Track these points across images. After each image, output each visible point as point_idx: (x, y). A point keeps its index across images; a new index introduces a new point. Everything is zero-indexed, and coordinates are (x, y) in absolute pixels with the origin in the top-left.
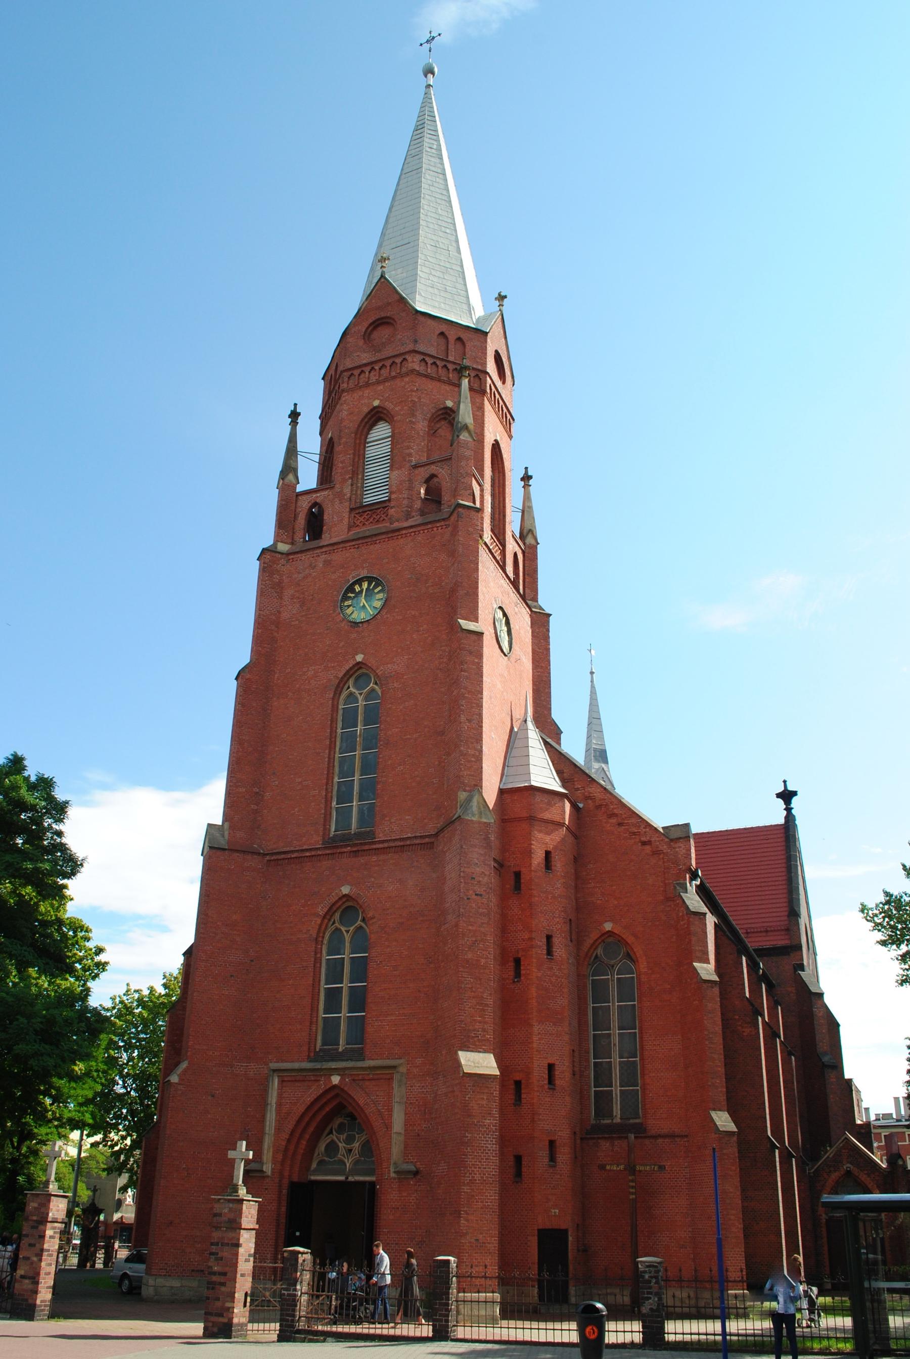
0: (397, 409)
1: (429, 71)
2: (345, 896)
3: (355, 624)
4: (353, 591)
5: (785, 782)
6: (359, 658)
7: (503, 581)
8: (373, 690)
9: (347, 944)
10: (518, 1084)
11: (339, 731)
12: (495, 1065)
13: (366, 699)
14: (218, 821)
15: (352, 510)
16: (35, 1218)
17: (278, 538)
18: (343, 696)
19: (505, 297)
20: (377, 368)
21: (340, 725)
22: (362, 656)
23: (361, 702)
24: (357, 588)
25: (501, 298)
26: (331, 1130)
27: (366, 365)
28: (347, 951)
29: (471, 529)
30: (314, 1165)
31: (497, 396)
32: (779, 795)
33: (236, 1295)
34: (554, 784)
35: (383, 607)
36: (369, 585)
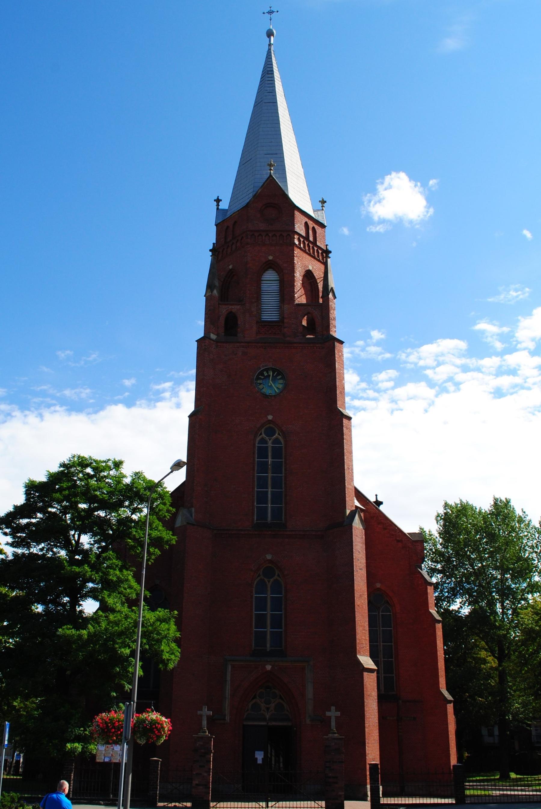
0: (285, 265)
1: (270, 34)
2: (268, 560)
3: (266, 396)
4: (263, 375)
5: (376, 495)
8: (277, 439)
9: (269, 589)
12: (373, 663)
16: (202, 751)
18: (258, 439)
19: (325, 202)
22: (272, 417)
23: (270, 444)
25: (323, 202)
28: (269, 593)
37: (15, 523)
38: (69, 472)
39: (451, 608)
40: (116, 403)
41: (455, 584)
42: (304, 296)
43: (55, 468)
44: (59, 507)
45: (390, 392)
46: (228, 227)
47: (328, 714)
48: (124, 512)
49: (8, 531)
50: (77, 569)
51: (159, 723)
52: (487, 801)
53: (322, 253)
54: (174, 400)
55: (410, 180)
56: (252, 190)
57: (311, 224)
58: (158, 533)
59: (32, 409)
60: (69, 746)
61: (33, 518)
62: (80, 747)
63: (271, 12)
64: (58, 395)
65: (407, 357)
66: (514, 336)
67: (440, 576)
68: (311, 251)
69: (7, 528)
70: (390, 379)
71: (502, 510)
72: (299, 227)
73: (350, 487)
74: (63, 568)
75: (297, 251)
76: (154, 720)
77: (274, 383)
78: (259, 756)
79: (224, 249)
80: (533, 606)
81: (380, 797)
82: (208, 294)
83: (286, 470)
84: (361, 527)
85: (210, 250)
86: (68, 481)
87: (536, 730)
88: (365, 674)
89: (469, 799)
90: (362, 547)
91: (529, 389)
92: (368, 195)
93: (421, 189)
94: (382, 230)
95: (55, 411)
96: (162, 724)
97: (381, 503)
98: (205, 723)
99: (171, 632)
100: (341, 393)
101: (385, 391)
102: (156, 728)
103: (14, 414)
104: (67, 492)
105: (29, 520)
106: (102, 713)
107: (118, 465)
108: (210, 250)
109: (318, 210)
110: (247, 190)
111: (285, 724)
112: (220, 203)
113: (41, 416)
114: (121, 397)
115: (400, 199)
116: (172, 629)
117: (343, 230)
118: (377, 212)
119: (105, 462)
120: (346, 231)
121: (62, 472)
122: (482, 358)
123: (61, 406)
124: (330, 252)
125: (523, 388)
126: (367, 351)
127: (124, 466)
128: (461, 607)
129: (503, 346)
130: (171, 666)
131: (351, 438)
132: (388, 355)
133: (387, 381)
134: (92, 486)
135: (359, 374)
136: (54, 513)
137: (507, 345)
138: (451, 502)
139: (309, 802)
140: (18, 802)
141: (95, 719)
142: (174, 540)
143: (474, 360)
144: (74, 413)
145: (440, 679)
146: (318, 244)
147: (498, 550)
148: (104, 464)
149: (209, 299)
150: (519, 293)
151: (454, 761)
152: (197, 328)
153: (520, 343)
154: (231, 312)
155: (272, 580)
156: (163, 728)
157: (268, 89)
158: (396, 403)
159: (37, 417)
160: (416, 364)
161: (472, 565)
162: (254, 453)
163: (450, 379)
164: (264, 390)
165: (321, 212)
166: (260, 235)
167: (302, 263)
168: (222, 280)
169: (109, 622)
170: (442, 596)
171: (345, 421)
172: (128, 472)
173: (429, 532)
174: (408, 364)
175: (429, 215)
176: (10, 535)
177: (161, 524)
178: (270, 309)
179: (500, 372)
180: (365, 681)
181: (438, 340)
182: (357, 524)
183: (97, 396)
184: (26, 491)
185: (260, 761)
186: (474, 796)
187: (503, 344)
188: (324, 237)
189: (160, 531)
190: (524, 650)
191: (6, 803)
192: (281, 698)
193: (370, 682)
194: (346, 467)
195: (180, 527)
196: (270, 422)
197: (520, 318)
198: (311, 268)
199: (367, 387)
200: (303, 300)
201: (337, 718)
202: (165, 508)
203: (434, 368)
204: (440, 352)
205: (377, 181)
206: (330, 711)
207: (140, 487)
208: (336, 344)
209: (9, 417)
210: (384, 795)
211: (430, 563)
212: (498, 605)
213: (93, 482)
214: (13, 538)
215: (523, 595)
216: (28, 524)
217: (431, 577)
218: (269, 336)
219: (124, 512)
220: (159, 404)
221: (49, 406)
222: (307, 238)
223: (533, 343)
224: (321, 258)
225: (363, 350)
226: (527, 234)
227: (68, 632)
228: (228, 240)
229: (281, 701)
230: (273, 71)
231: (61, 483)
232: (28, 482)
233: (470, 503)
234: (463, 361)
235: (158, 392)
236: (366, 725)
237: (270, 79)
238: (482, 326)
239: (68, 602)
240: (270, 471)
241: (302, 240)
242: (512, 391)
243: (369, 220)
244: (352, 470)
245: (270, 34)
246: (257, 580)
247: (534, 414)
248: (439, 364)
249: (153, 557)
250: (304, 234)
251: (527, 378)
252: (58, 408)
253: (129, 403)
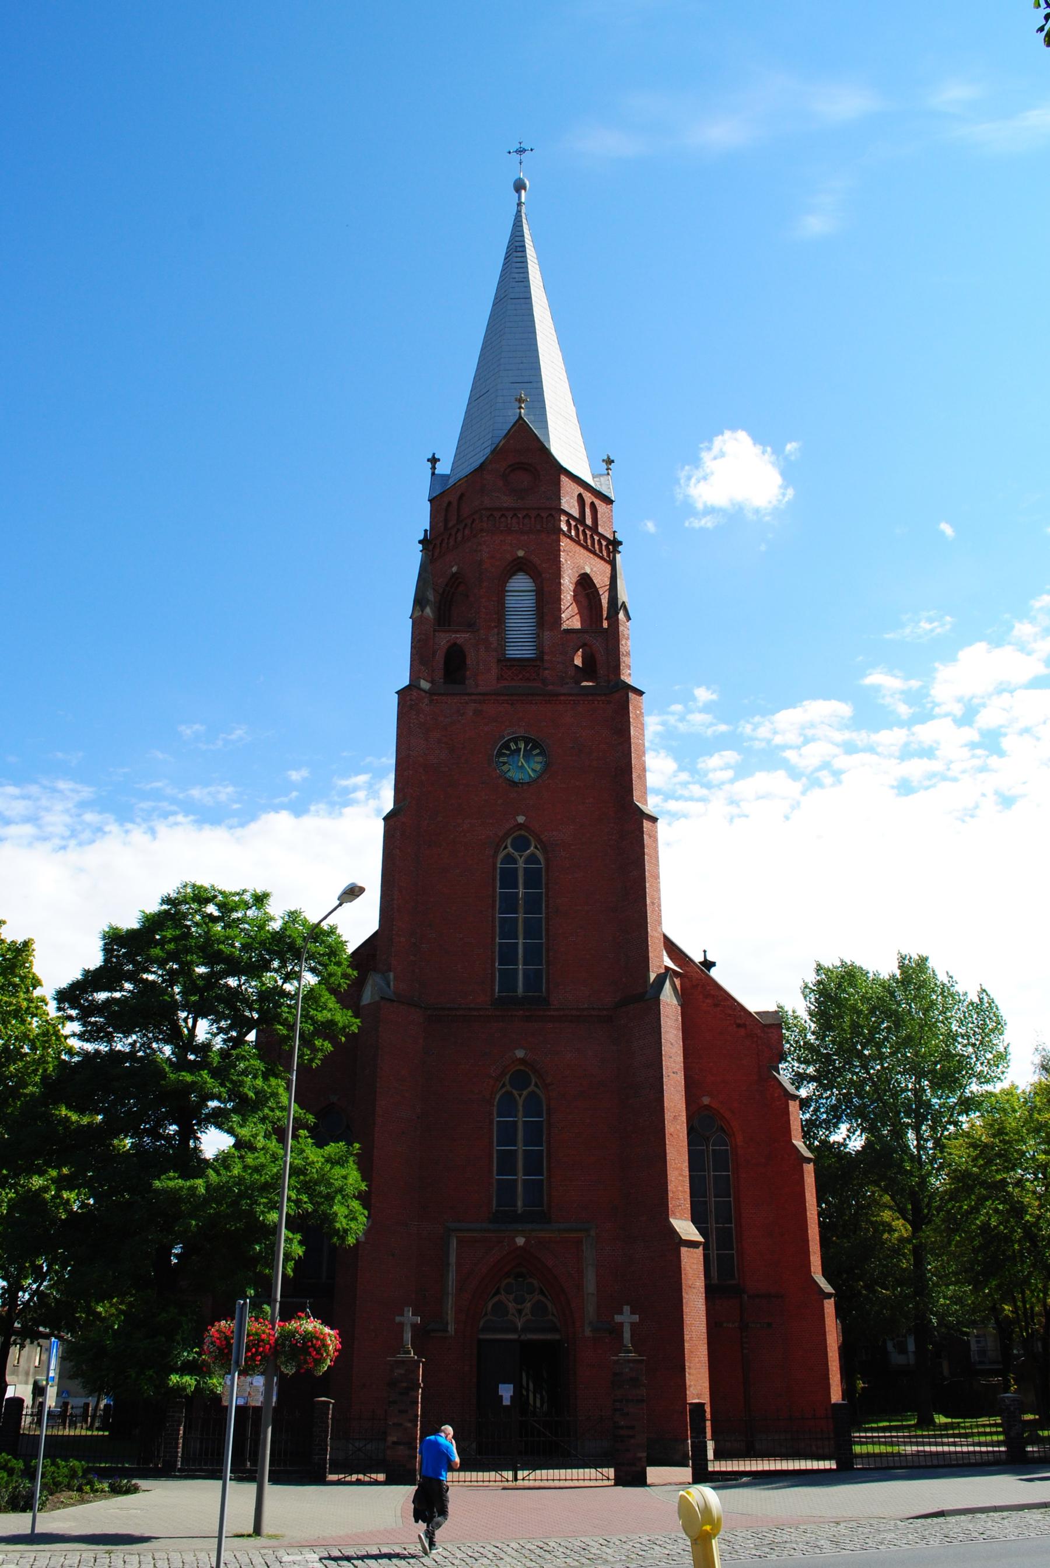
1: (519, 186)
3: (513, 784)
4: (508, 748)
5: (705, 951)
8: (533, 855)
9: (520, 1108)
13: (526, 862)
16: (405, 1385)
18: (501, 856)
19: (613, 461)
23: (521, 864)
24: (513, 747)
25: (609, 462)
26: (498, 1288)
27: (508, 509)
28: (520, 1114)
37: (86, 1000)
38: (178, 912)
39: (832, 1139)
40: (277, 809)
41: (838, 1100)
42: (578, 617)
43: (154, 907)
44: (160, 972)
45: (727, 787)
46: (450, 503)
47: (618, 1318)
48: (270, 978)
49: (74, 1013)
50: (189, 1078)
51: (317, 1339)
52: (892, 1465)
53: (607, 546)
55: (755, 444)
56: (490, 442)
57: (588, 498)
58: (329, 1015)
59: (138, 820)
60: (174, 1378)
61: (116, 991)
62: (193, 1383)
63: (521, 151)
64: (181, 796)
65: (754, 730)
66: (928, 695)
67: (813, 1086)
68: (589, 541)
69: (72, 1007)
70: (727, 767)
71: (914, 975)
72: (567, 502)
73: (656, 935)
74: (163, 1075)
75: (564, 543)
76: (310, 1333)
77: (527, 761)
78: (506, 1392)
79: (443, 540)
80: (968, 1133)
81: (707, 1460)
82: (417, 614)
83: (547, 907)
84: (675, 1002)
85: (420, 542)
86: (176, 927)
87: (978, 1342)
88: (684, 1250)
89: (859, 1460)
90: (676, 1036)
91: (955, 780)
92: (687, 468)
93: (773, 458)
94: (709, 525)
95: (177, 824)
96: (324, 1339)
97: (713, 964)
98: (408, 1336)
99: (350, 1181)
100: (639, 777)
101: (720, 785)
102: (313, 1346)
103: (107, 829)
104: (172, 946)
105: (109, 994)
106: (219, 1321)
107: (260, 899)
108: (420, 542)
109: (601, 475)
110: (482, 441)
111: (549, 1336)
112: (438, 464)
113: (153, 832)
114: (285, 800)
115: (738, 475)
116: (352, 1177)
117: (645, 525)
118: (700, 496)
119: (238, 894)
120: (650, 526)
121: (166, 912)
122: (876, 730)
123: (186, 815)
124: (620, 543)
125: (945, 778)
126: (688, 721)
127: (271, 901)
128: (848, 1137)
129: (911, 711)
130: (351, 1240)
131: (657, 858)
132: (723, 728)
133: (722, 769)
134: (215, 935)
135: (676, 759)
136: (154, 982)
137: (918, 710)
138: (827, 963)
139: (587, 1470)
140: (83, 1477)
141: (208, 1331)
142: (355, 1025)
143: (863, 734)
144: (207, 827)
145: (812, 1258)
146: (600, 530)
147: (908, 1042)
148: (237, 898)
149: (418, 623)
150: (936, 624)
151: (836, 1396)
152: (397, 671)
153: (939, 705)
154: (455, 644)
155: (525, 1093)
156: (325, 1345)
157: (516, 276)
158: (738, 806)
159: (145, 833)
160: (769, 741)
161: (865, 1067)
162: (494, 880)
163: (826, 765)
164: (510, 774)
165: (606, 477)
166: (503, 515)
167: (574, 562)
168: (441, 591)
169: (245, 1167)
170: (816, 1120)
171: (646, 824)
172: (277, 911)
173: (794, 1012)
174: (757, 742)
175: (786, 499)
176: (79, 1020)
177: (333, 999)
178: (520, 639)
179: (906, 753)
180: (683, 1263)
181: (805, 703)
182: (668, 997)
183: (245, 797)
184: (106, 944)
185: (507, 1402)
186: (869, 1455)
187: (910, 708)
188: (610, 518)
189: (331, 1010)
190: (954, 1206)
191: (60, 1479)
192: (542, 1292)
193: (692, 1265)
194: (648, 901)
195: (369, 1004)
196: (520, 826)
197: (936, 665)
198: (588, 571)
199: (690, 779)
200: (576, 623)
201: (632, 1324)
202: (339, 971)
203: (799, 748)
204: (808, 722)
205: (701, 446)
206: (621, 1313)
207: (295, 935)
208: (631, 695)
209: (100, 834)
210: (719, 1456)
211: (796, 1064)
212: (911, 1135)
213: (218, 927)
214: (84, 1025)
215: (952, 1115)
216: (108, 1002)
217: (798, 1088)
218: (518, 686)
219: (270, 978)
220: (347, 811)
221: (166, 815)
222: (581, 520)
223: (960, 705)
224: (605, 553)
225: (682, 719)
226: (947, 529)
227: (171, 1184)
228: (450, 524)
229: (543, 1299)
230: (524, 246)
231: (163, 931)
232: (107, 930)
233: (857, 964)
234: (847, 735)
235: (346, 791)
236: (686, 1337)
237: (519, 260)
238: (876, 678)
239: (176, 1133)
240: (521, 910)
241: (573, 523)
242: (927, 783)
243: (688, 509)
244: (659, 905)
245: (519, 186)
246: (501, 1093)
247: (964, 821)
248: (807, 741)
249: (320, 1055)
250: (576, 514)
251: (951, 762)
252: (180, 818)
253: (299, 809)
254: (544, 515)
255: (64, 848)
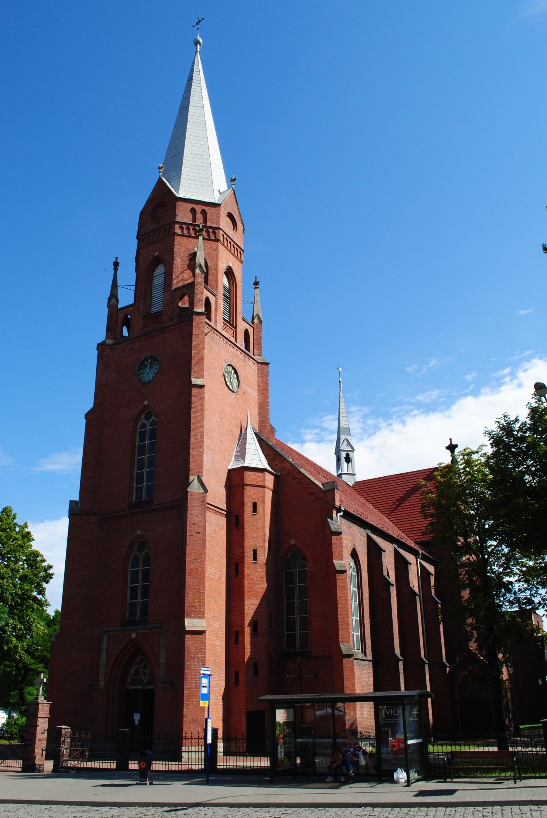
2: (138, 536)
3: (144, 384)
5: (451, 439)
6: (146, 403)
7: (232, 349)
10: (237, 632)
11: (137, 444)
13: (151, 426)
14: (77, 499)
15: (144, 317)
17: (107, 337)
18: (139, 425)
20: (157, 233)
21: (138, 441)
23: (148, 428)
28: (141, 565)
29: (200, 326)
30: (129, 681)
31: (229, 240)
32: (448, 448)
33: (36, 750)
34: (263, 463)
35: (158, 372)
36: (151, 361)
40: (465, 395)
54: (515, 382)
64: (413, 401)
95: (415, 416)
114: (467, 391)
144: (431, 413)
196: (146, 407)
220: (502, 388)
221: (408, 412)
252: (415, 412)
253: (476, 393)
254: (167, 228)
255: (362, 439)
